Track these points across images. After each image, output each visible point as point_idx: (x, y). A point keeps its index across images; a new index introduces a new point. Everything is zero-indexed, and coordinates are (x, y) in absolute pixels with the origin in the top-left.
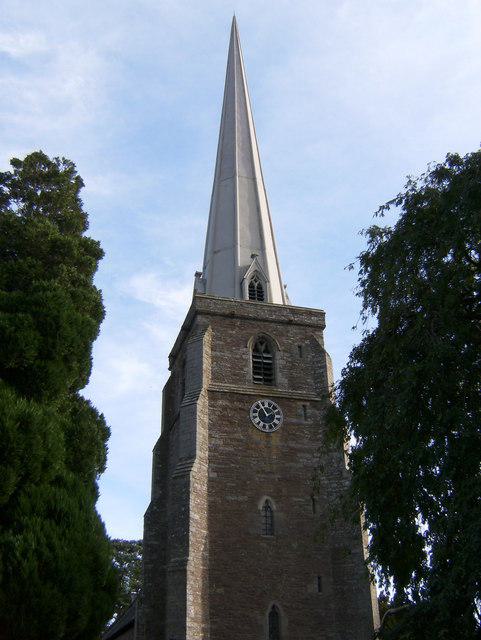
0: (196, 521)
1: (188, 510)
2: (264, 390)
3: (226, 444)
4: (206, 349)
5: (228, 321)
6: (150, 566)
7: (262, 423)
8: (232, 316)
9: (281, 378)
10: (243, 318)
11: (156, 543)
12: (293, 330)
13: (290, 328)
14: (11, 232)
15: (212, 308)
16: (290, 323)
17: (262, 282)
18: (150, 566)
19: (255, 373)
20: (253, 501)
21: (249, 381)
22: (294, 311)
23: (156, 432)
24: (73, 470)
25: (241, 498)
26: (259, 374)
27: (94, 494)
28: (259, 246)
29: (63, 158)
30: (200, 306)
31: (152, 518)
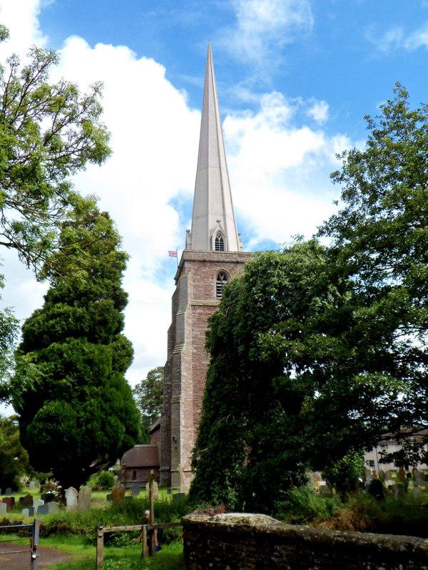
0: (185, 377)
1: (180, 371)
4: (190, 282)
8: (204, 261)
14: (48, 189)
16: (238, 262)
19: (218, 293)
23: (170, 322)
24: (79, 317)
26: (220, 293)
27: (157, 61)
30: (187, 257)
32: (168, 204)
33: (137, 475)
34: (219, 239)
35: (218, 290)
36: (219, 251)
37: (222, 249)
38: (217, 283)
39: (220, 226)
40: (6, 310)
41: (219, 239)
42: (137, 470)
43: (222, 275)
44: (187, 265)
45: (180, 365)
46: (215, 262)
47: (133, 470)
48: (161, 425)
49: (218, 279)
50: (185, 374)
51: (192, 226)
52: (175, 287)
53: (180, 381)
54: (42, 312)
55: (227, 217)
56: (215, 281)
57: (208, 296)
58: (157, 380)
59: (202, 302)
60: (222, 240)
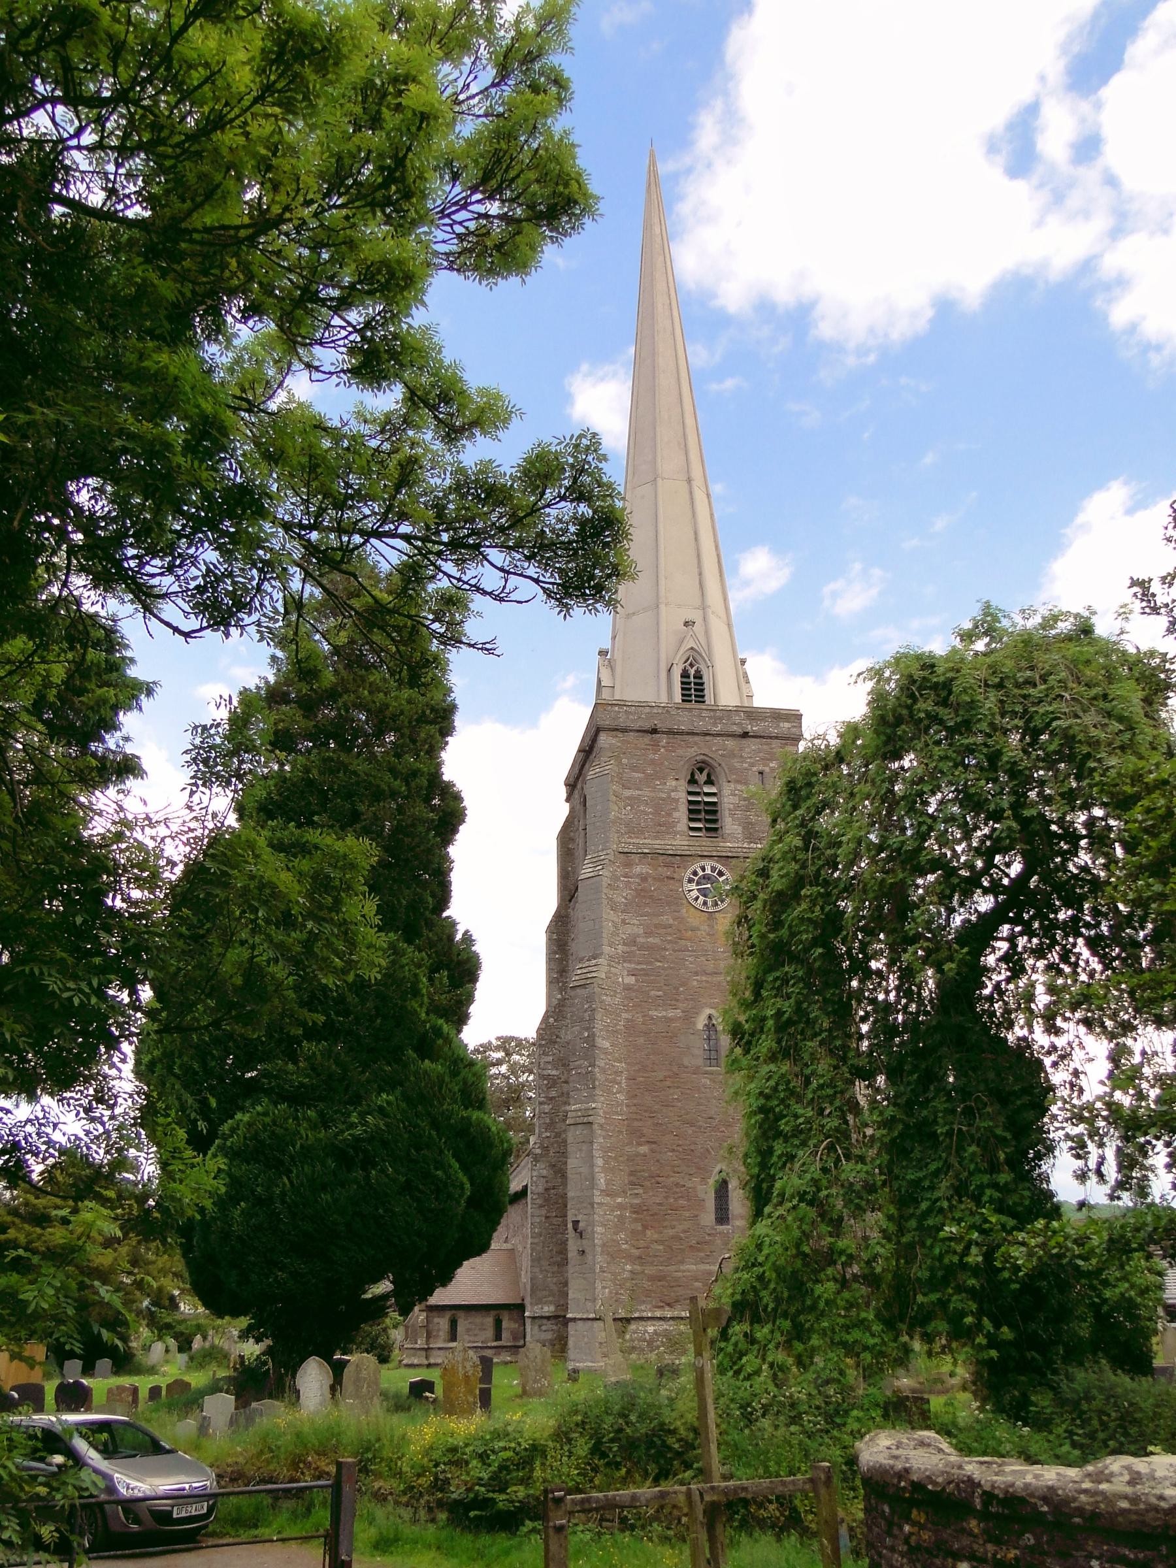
1: (592, 1037)
2: (704, 843)
3: (648, 934)
5: (647, 739)
6: (547, 1108)
7: (701, 898)
9: (730, 825)
10: (671, 732)
11: (554, 1072)
12: (752, 745)
13: (744, 741)
15: (622, 721)
16: (745, 735)
17: (702, 667)
18: (547, 1108)
20: (689, 1017)
21: (681, 833)
22: (754, 714)
23: (549, 903)
25: (671, 1014)
28: (698, 603)
29: (466, 932)
31: (516, 1193)
33: (460, 1329)
34: (692, 672)
35: (690, 811)
36: (693, 705)
37: (700, 698)
38: (690, 793)
39: (695, 637)
41: (692, 672)
42: (461, 1316)
43: (701, 770)
45: (592, 1019)
46: (682, 733)
47: (448, 1315)
49: (692, 781)
50: (606, 1044)
51: (614, 638)
52: (564, 810)
53: (593, 1065)
54: (274, 696)
55: (710, 611)
56: (683, 785)
57: (665, 827)
58: (494, 1071)
59: (649, 843)
60: (698, 675)
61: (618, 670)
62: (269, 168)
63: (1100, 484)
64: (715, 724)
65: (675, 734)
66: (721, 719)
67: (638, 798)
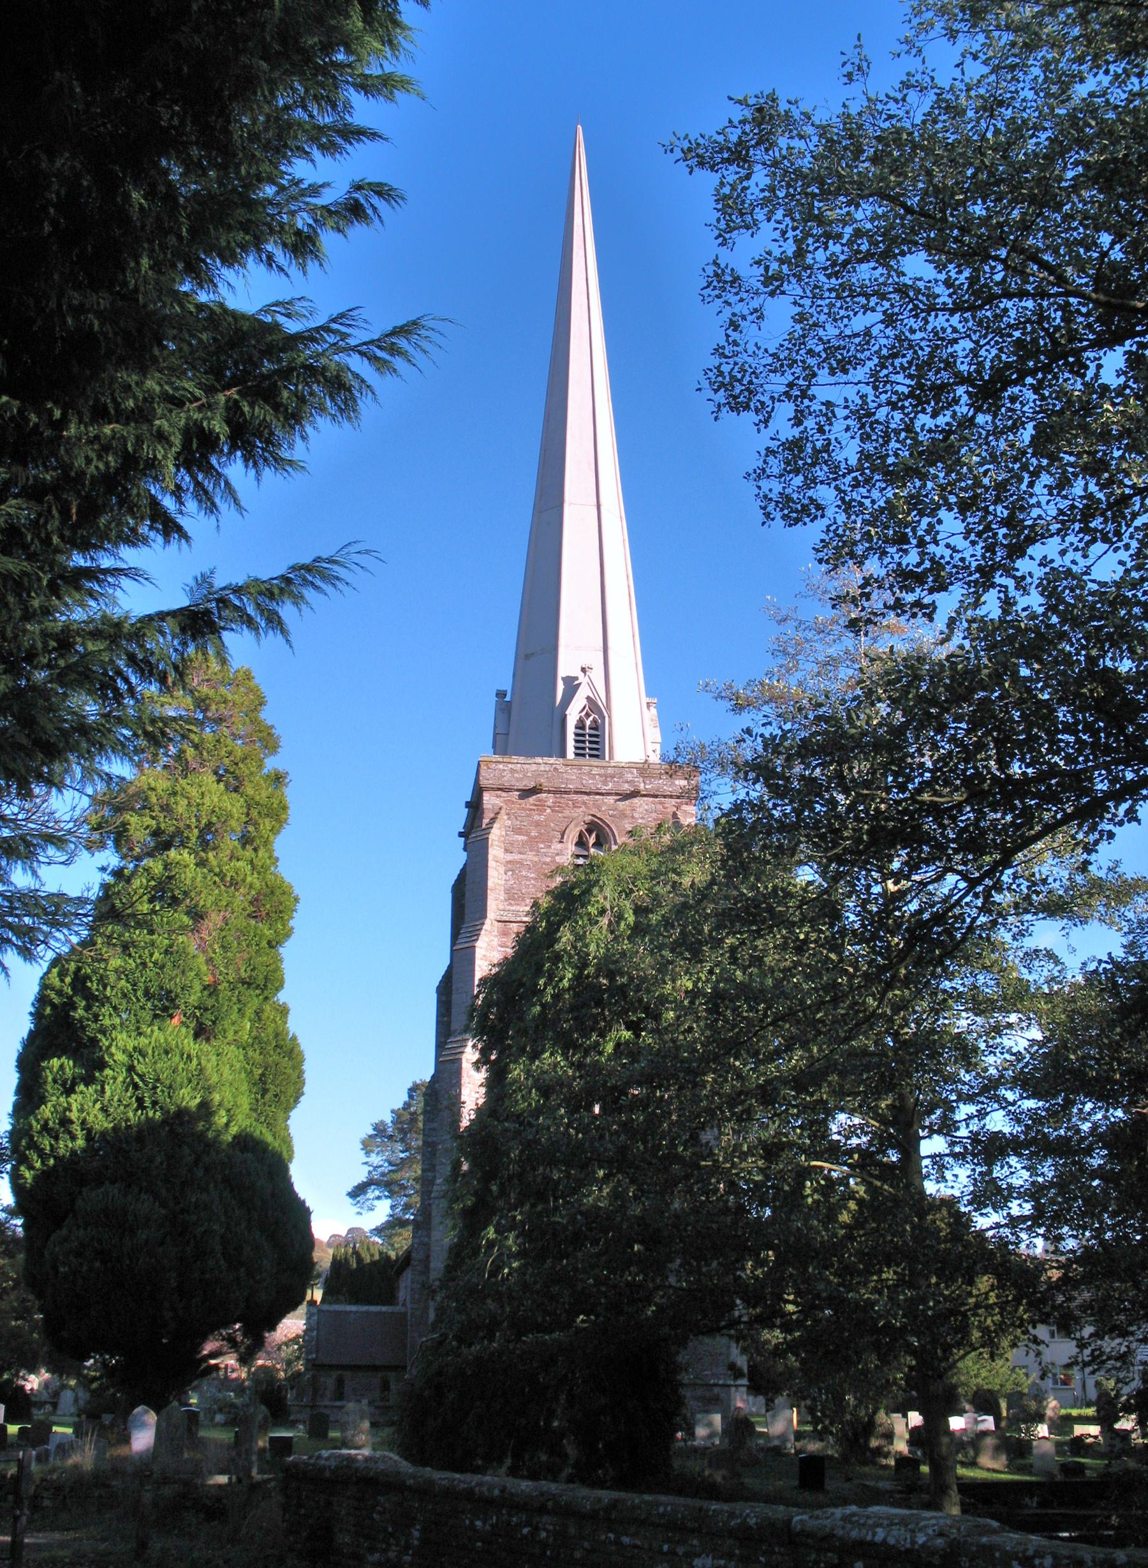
10: (557, 792)
32: (1139, 821)
34: (588, 723)
40: (583, 670)
42: (348, 1374)
43: (590, 831)
44: (489, 800)
47: (335, 1374)
48: (414, 1255)
49: (581, 843)
52: (463, 857)
60: (595, 726)
61: (514, 717)
62: (736, 327)
63: (141, 1455)
64: (605, 783)
65: (561, 792)
66: (612, 777)
67: (520, 863)
